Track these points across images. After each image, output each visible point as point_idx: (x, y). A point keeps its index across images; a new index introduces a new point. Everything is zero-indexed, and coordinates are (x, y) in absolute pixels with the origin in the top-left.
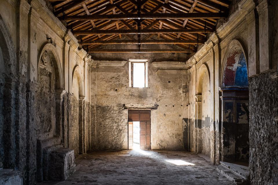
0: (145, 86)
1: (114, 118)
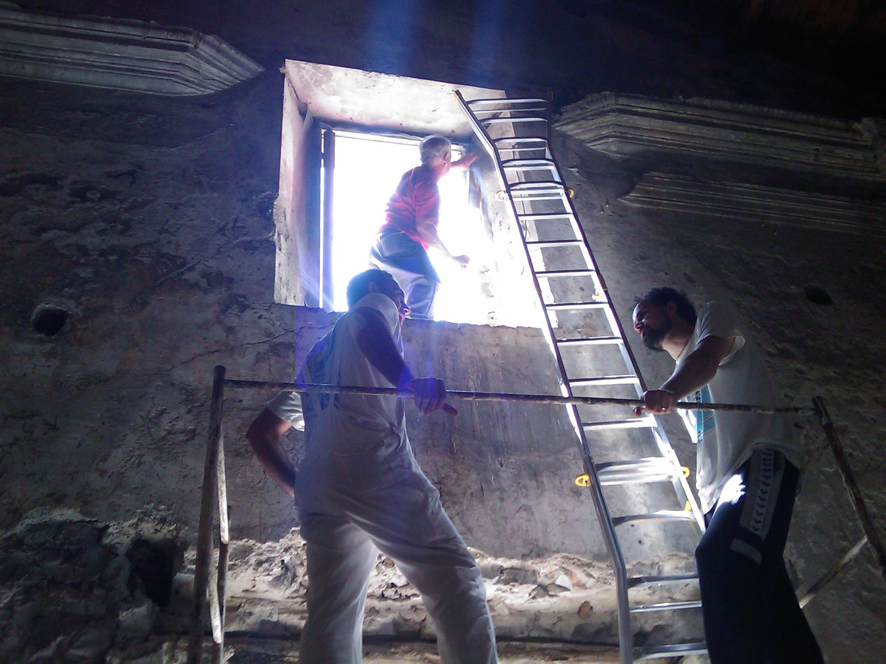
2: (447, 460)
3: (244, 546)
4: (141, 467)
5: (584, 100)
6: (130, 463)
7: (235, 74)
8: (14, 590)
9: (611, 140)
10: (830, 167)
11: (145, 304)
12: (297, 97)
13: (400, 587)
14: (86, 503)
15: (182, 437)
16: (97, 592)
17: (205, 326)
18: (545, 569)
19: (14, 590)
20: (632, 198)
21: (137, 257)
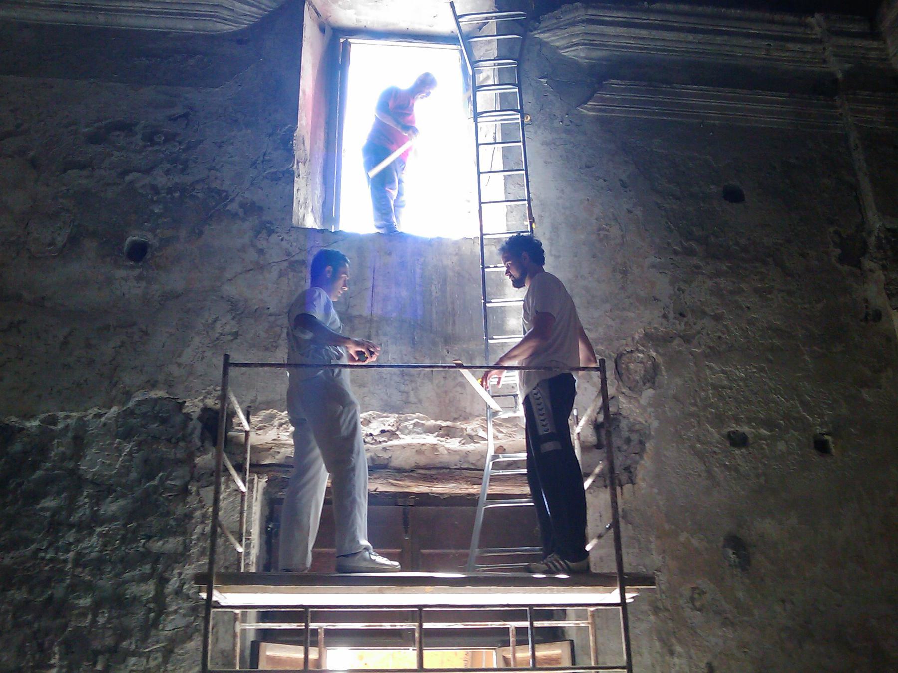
0: (237, 365)
1: (59, 591)
2: (409, 349)
3: (270, 413)
4: (204, 360)
5: (560, 10)
6: (196, 357)
7: (263, 7)
8: (132, 443)
9: (581, 47)
10: (779, 61)
11: (201, 233)
12: (317, 13)
13: (376, 436)
14: (170, 386)
15: (230, 338)
16: (182, 444)
17: (243, 249)
18: (471, 427)
19: (132, 443)
20: (590, 106)
21: (194, 193)
